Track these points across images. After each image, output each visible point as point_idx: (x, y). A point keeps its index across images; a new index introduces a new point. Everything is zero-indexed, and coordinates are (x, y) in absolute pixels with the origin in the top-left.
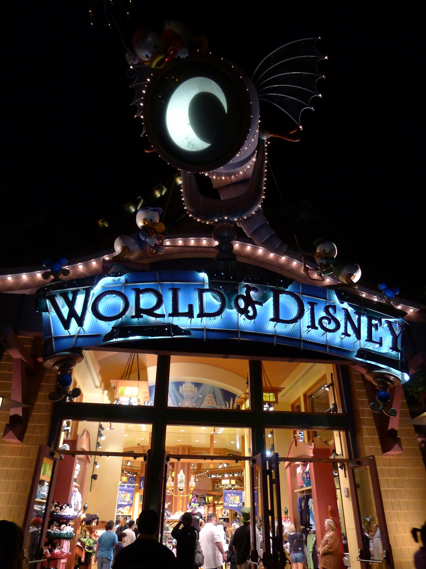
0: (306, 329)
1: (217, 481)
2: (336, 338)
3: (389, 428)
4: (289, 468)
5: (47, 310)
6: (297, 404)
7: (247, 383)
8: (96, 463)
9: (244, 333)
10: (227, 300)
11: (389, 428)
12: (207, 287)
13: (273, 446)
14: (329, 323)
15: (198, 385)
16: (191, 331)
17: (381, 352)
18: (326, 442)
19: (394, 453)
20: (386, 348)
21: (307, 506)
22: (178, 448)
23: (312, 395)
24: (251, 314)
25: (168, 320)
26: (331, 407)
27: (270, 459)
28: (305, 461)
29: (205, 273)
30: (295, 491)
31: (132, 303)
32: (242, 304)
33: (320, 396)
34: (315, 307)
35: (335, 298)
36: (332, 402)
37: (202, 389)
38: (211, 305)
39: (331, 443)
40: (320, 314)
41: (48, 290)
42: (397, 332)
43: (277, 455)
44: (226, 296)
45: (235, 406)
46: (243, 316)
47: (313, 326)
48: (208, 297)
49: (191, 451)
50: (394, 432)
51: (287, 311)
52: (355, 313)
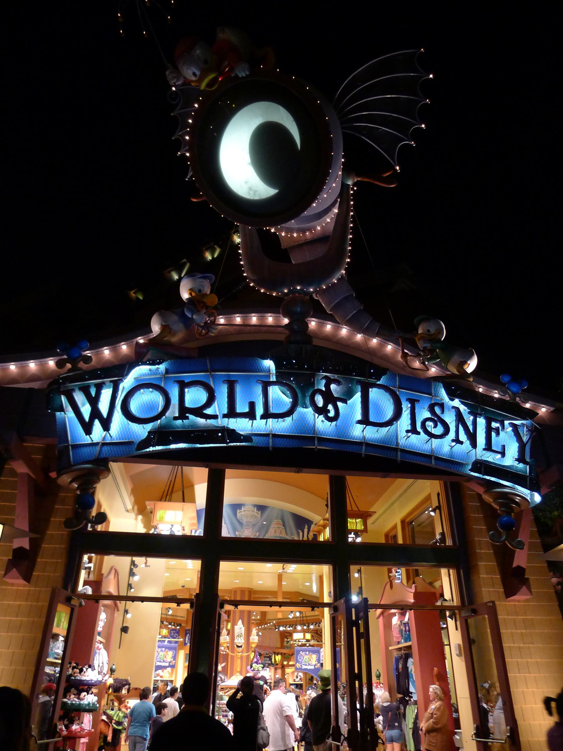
0: (404, 435)
1: (287, 635)
2: (445, 447)
3: (515, 565)
4: (381, 617)
5: (62, 409)
6: (392, 534)
7: (327, 505)
8: (126, 612)
9: (322, 440)
10: (300, 395)
11: (515, 565)
12: (273, 379)
13: (361, 588)
14: (435, 426)
15: (261, 508)
16: (253, 437)
17: (504, 464)
18: (431, 584)
19: (521, 598)
20: (510, 460)
21: (406, 668)
22: (235, 591)
23: (412, 522)
24: (332, 414)
25: (222, 422)
26: (438, 537)
27: (356, 606)
28: (403, 608)
29: (270, 360)
30: (390, 648)
31: (175, 400)
32: (320, 401)
33: (423, 523)
34: (417, 405)
35: (443, 393)
36: (438, 530)
37: (267, 513)
38: (278, 402)
39: (437, 584)
40: (423, 414)
41: (64, 383)
42: (525, 439)
43: (366, 600)
44: (298, 391)
45: (311, 536)
46: (321, 417)
47: (414, 430)
48: (275, 392)
49: (253, 596)
50: (520, 571)
51: (379, 411)
52: (469, 413)
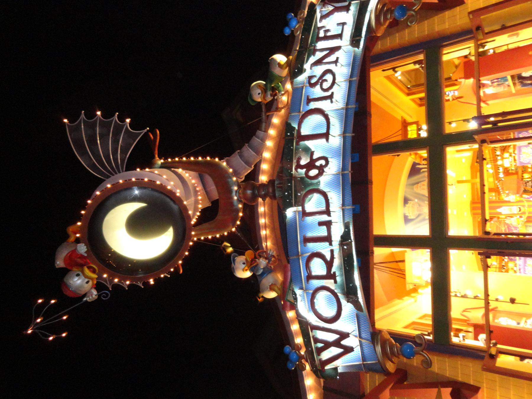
0: (337, 103)
1: (507, 172)
2: (342, 71)
4: (488, 102)
5: (336, 369)
6: (419, 102)
7: (398, 155)
8: (497, 300)
9: (344, 168)
10: (311, 188)
12: (300, 208)
13: (464, 120)
14: (326, 80)
15: (406, 201)
16: (346, 221)
18: (457, 67)
20: (348, 17)
22: (474, 214)
23: (408, 88)
24: (323, 162)
26: (417, 66)
27: (480, 125)
28: (479, 86)
29: (286, 211)
30: (514, 92)
32: (313, 172)
33: (408, 79)
34: (311, 97)
36: (412, 67)
37: (409, 196)
39: (457, 62)
40: (317, 92)
41: (316, 367)
42: (331, 8)
43: (474, 118)
44: (308, 189)
45: (425, 162)
49: (476, 200)
51: (318, 126)
52: (314, 55)
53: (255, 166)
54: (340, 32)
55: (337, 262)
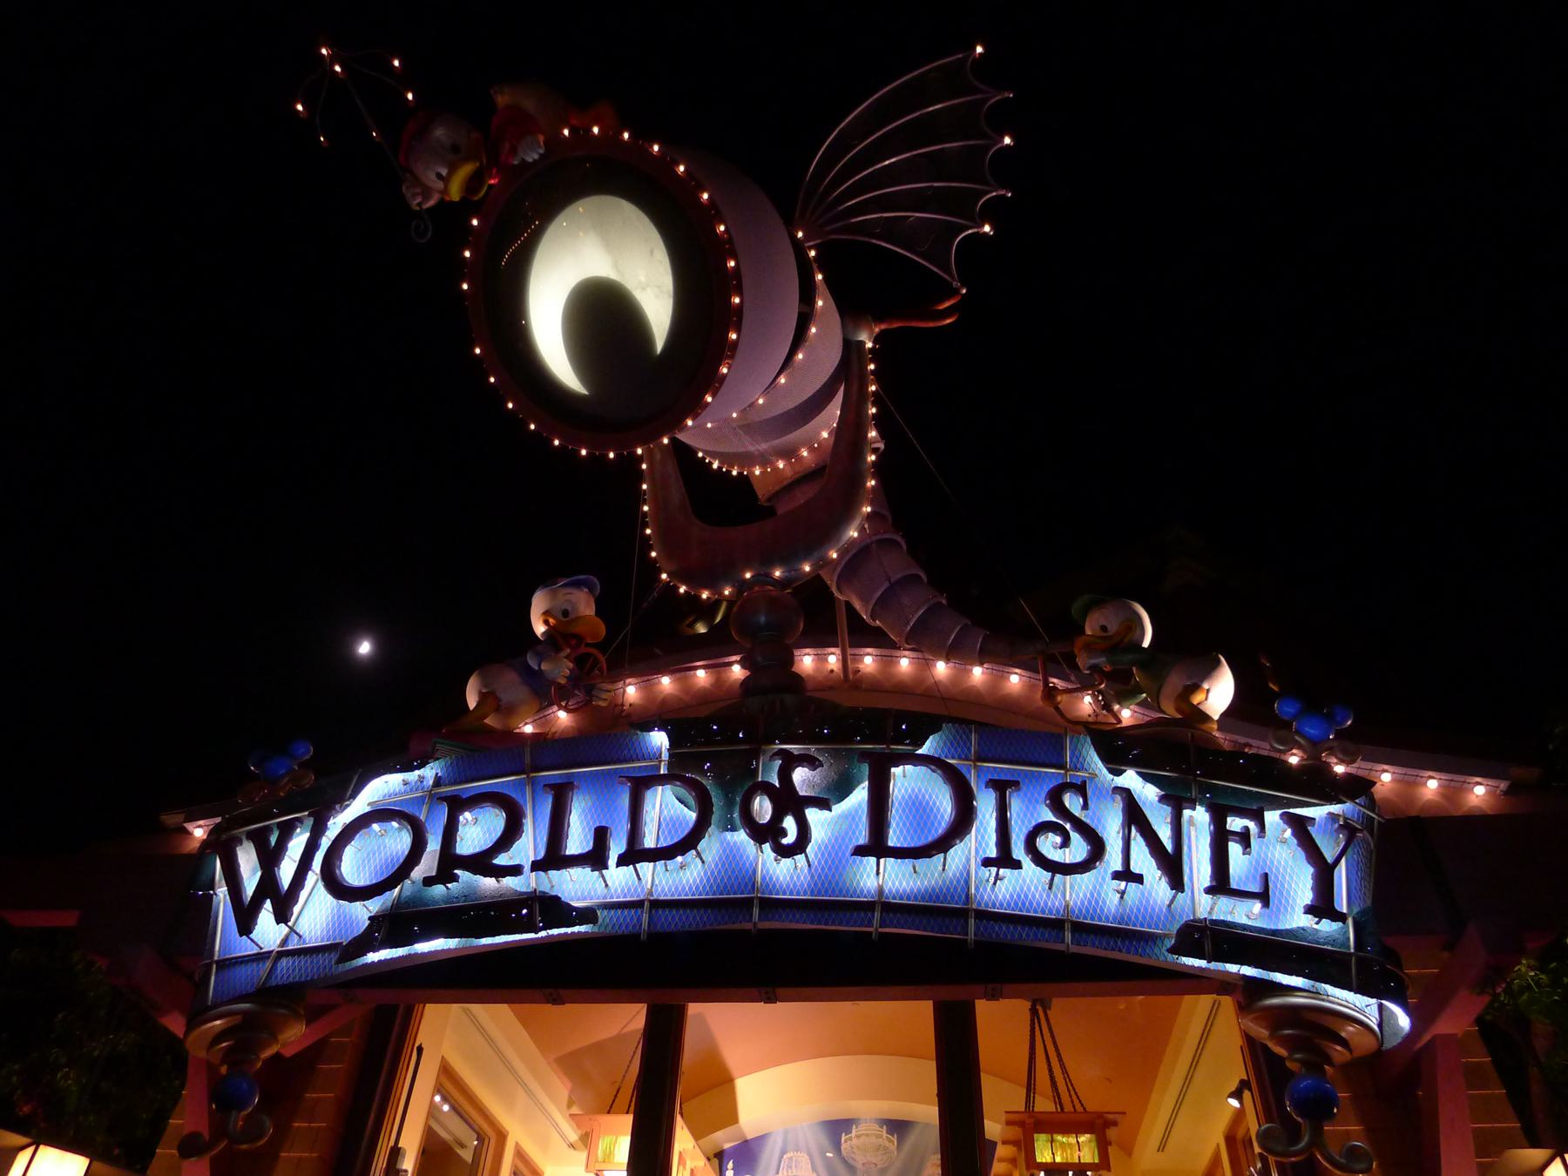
7: (420, 1050)
14: (1066, 843)
15: (898, 1127)
17: (1281, 927)
31: (434, 845)
32: (763, 808)
37: (912, 1138)
40: (1027, 811)
52: (1162, 799)
53: (878, 631)
54: (1234, 885)
55: (488, 883)
